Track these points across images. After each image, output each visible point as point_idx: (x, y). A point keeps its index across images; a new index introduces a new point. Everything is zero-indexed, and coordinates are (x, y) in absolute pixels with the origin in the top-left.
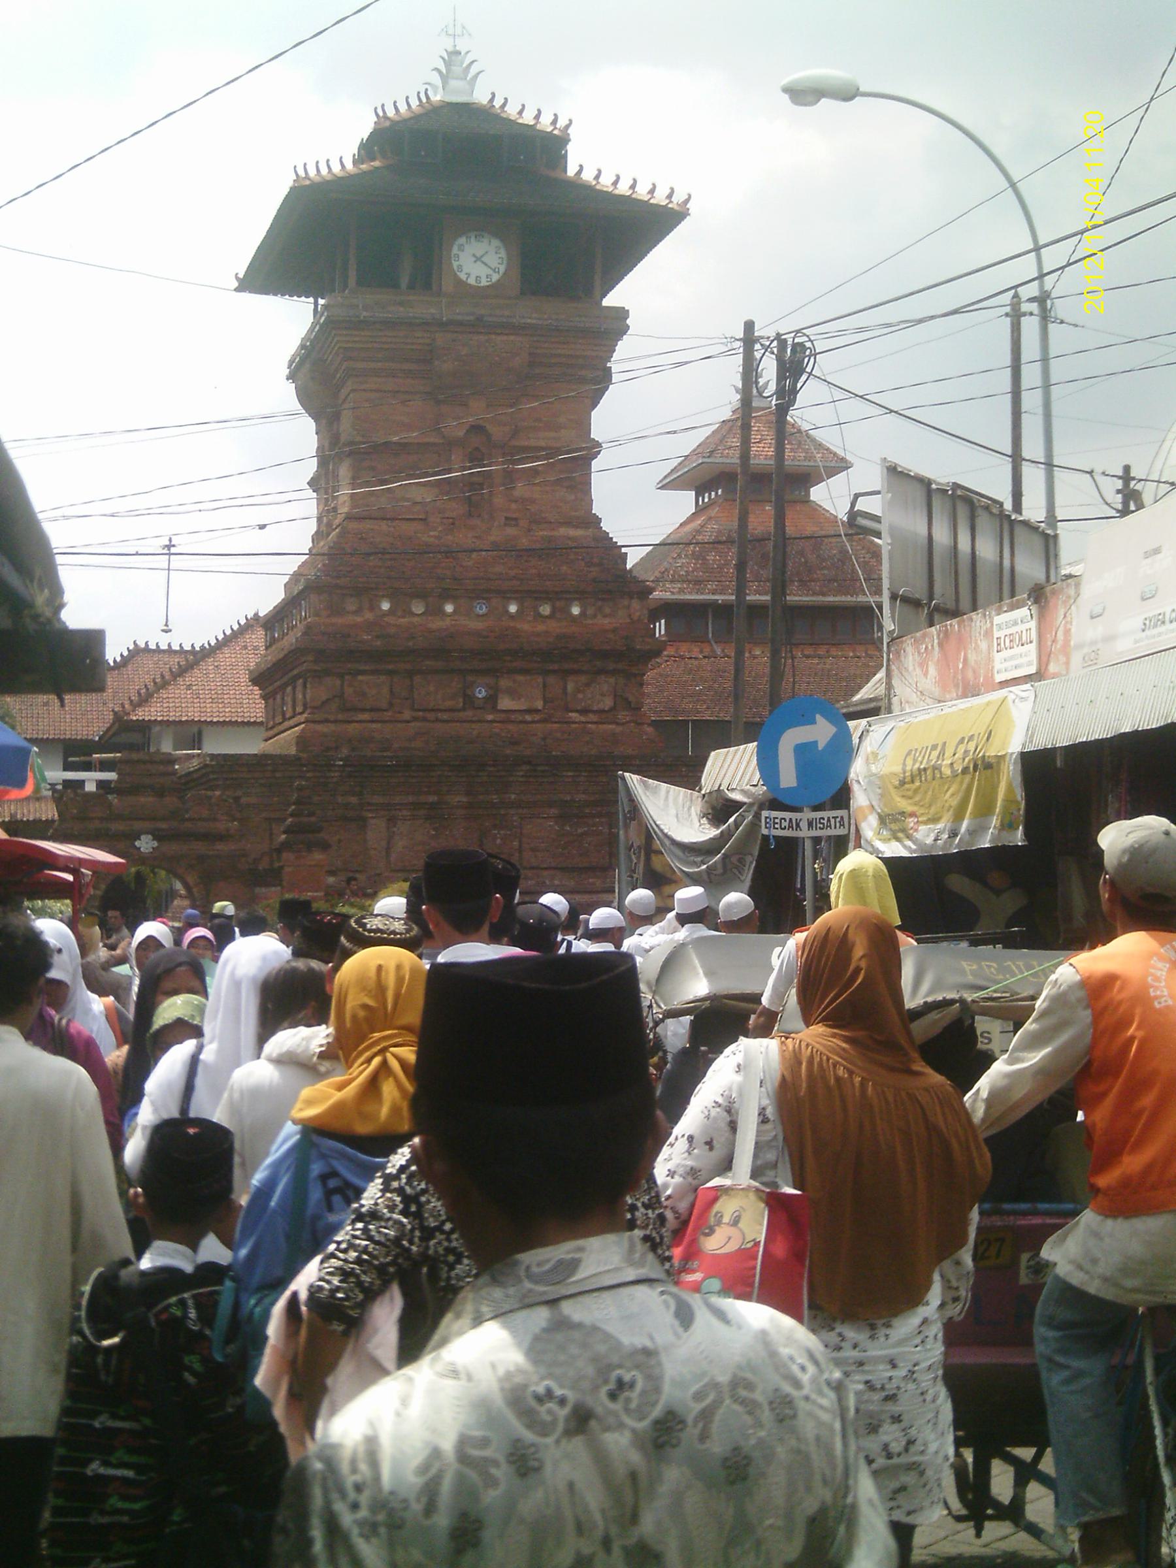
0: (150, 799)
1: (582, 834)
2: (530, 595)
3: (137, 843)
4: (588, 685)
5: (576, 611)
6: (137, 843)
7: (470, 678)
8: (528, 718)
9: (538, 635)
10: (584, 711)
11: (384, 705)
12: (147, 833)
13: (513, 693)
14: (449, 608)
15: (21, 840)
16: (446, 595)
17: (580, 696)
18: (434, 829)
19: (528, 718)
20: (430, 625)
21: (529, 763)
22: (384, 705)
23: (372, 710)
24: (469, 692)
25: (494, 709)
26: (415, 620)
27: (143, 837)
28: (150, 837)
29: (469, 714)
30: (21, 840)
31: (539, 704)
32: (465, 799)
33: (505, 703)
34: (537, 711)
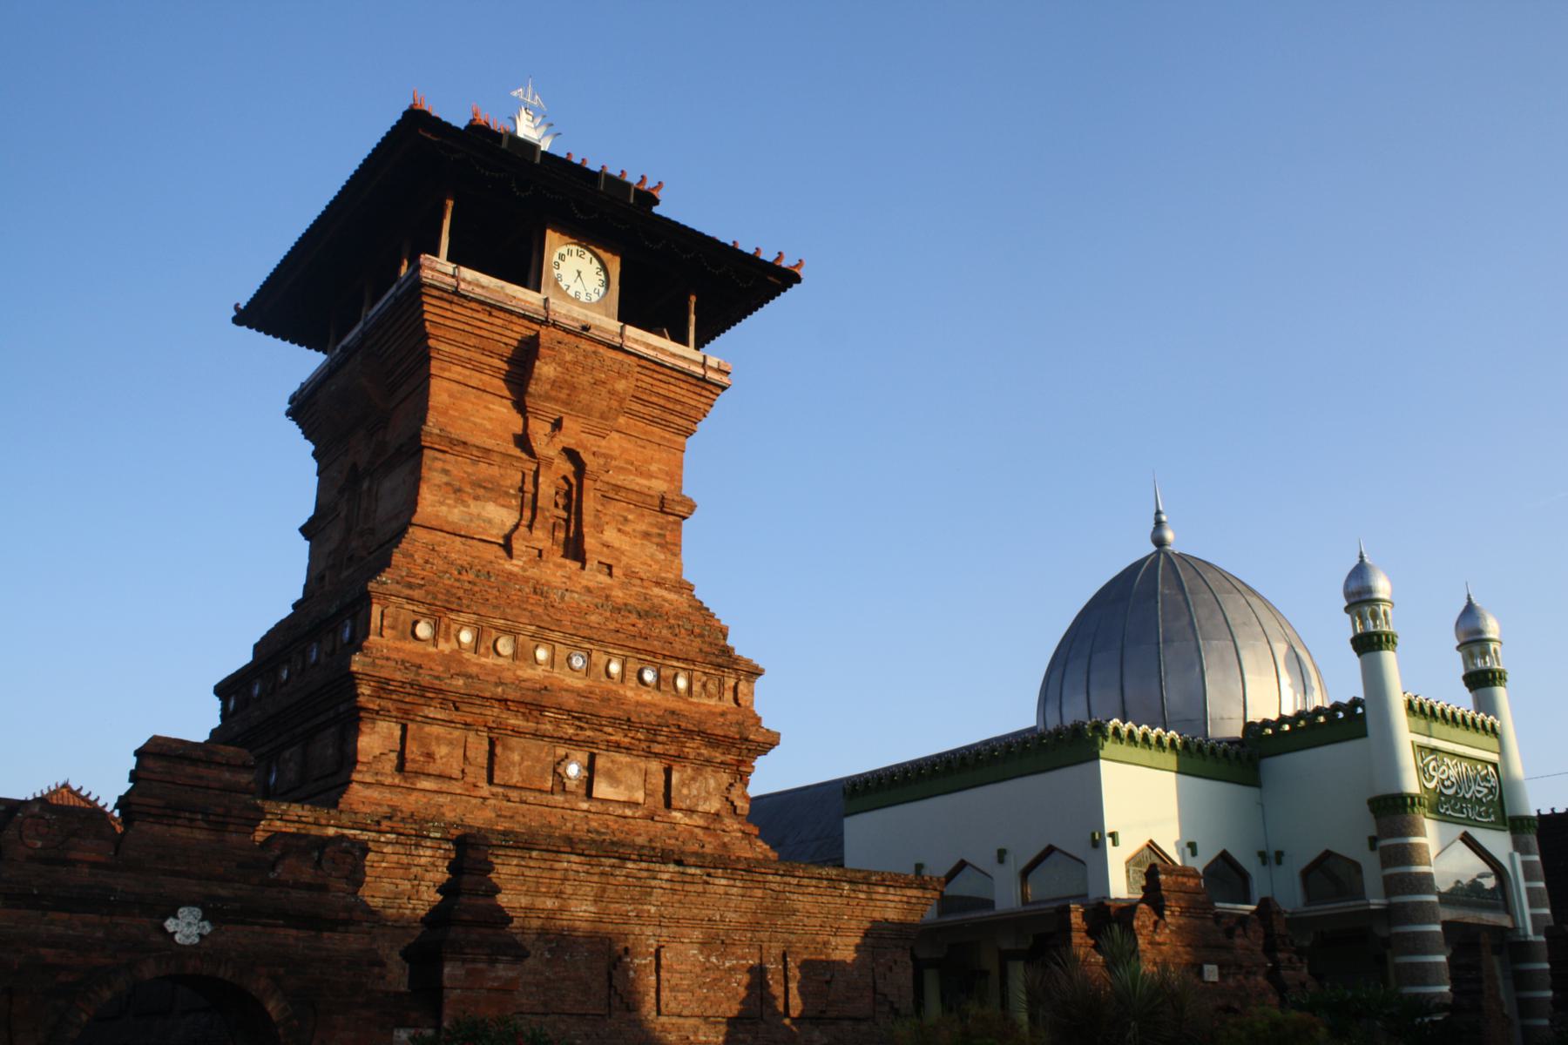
0: (200, 835)
1: (730, 969)
2: (641, 650)
3: (170, 925)
4: (693, 779)
5: (682, 683)
6: (170, 925)
7: (561, 751)
8: (628, 812)
9: (644, 705)
10: (690, 811)
11: (456, 773)
12: (191, 903)
13: (613, 780)
14: (542, 654)
15: (693, 318)
16: (539, 638)
17: (685, 791)
18: (550, 950)
19: (628, 812)
20: (519, 673)
21: (679, 863)
22: (456, 773)
23: (440, 776)
24: (560, 770)
25: (589, 794)
26: (500, 661)
27: (183, 911)
28: (197, 912)
29: (559, 798)
30: (693, 318)
31: (639, 796)
32: (593, 909)
33: (602, 789)
34: (637, 804)
